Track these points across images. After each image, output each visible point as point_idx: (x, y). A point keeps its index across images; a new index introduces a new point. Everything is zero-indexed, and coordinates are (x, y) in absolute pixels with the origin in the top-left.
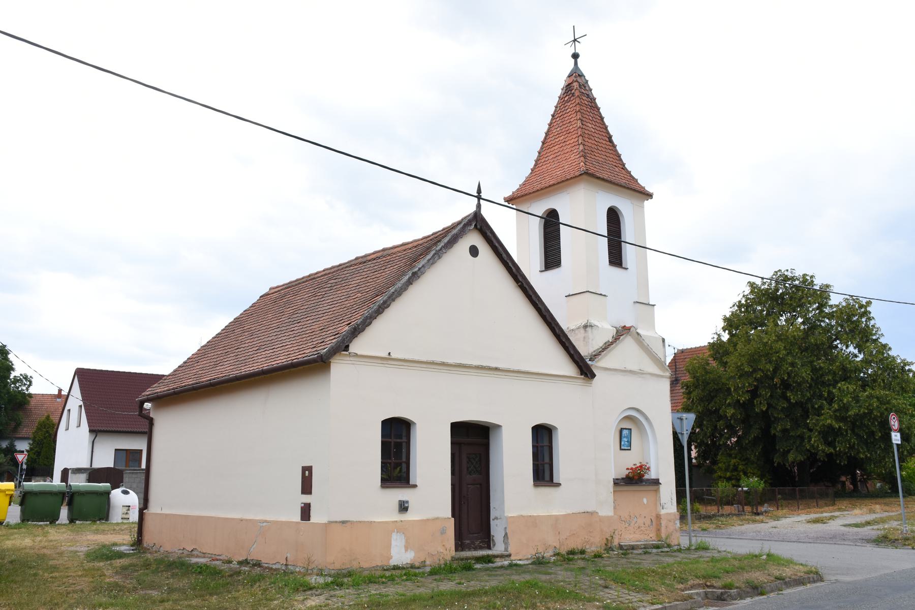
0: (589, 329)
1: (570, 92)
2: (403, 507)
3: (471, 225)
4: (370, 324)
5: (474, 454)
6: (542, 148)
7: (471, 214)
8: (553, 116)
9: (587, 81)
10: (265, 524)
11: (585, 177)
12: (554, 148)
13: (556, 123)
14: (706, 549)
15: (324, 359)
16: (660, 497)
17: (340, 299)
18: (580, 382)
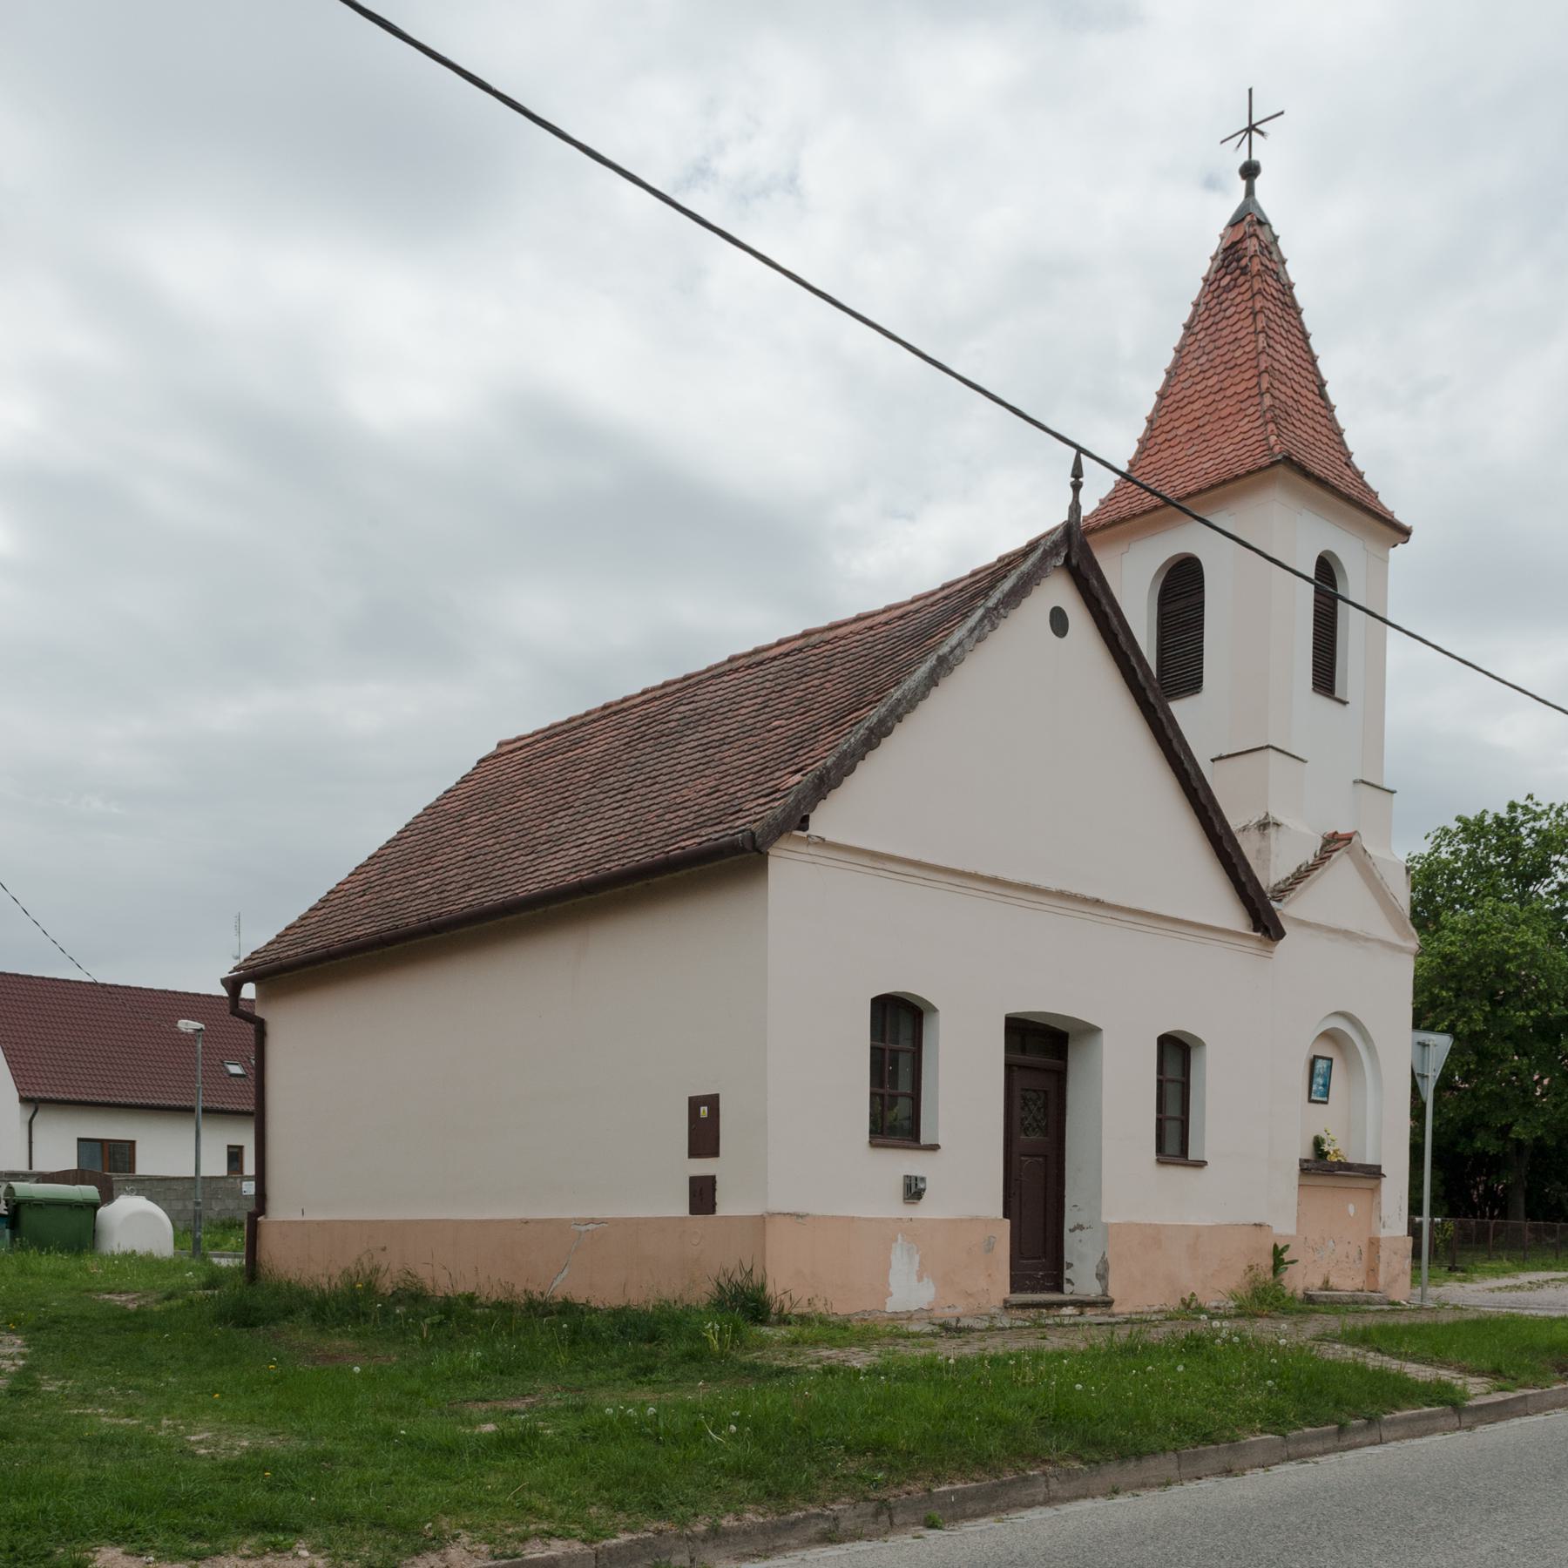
0: (1272, 831)
1: (1234, 264)
2: (913, 1190)
3: (1058, 554)
4: (852, 769)
5: (1035, 1091)
6: (1157, 409)
7: (1055, 529)
8: (1187, 327)
9: (1276, 238)
10: (590, 1227)
11: (1281, 469)
12: (1190, 407)
13: (1197, 344)
15: (757, 844)
16: (1379, 1203)
17: (534, 838)
18: (1253, 943)
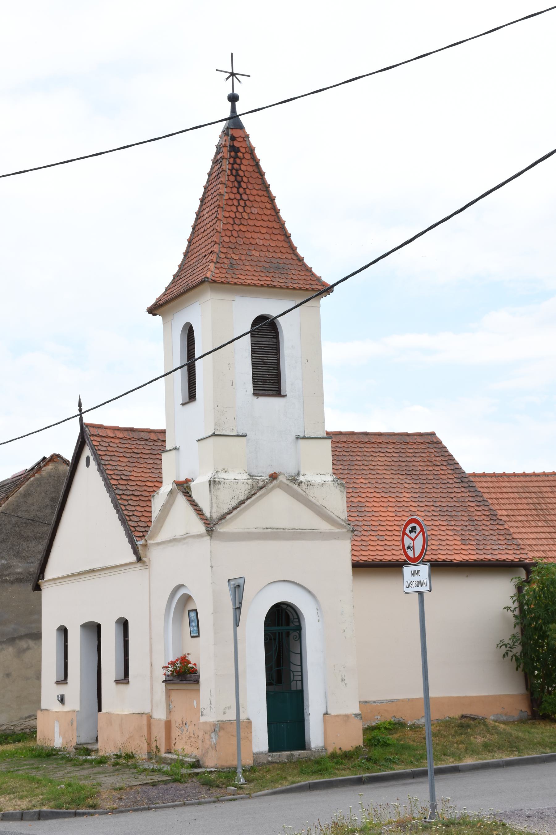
14: (271, 789)
